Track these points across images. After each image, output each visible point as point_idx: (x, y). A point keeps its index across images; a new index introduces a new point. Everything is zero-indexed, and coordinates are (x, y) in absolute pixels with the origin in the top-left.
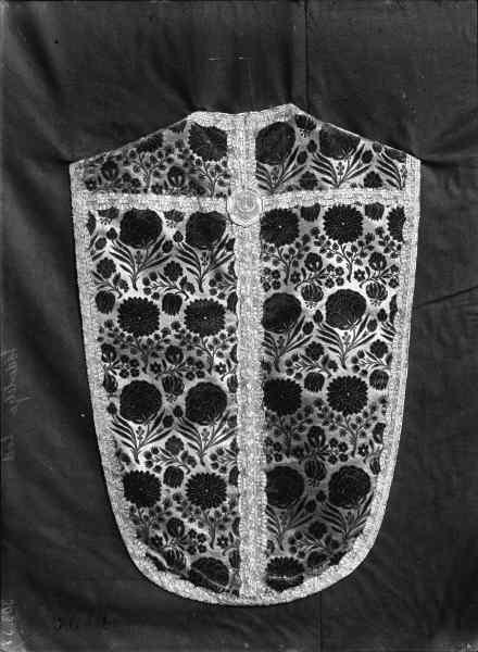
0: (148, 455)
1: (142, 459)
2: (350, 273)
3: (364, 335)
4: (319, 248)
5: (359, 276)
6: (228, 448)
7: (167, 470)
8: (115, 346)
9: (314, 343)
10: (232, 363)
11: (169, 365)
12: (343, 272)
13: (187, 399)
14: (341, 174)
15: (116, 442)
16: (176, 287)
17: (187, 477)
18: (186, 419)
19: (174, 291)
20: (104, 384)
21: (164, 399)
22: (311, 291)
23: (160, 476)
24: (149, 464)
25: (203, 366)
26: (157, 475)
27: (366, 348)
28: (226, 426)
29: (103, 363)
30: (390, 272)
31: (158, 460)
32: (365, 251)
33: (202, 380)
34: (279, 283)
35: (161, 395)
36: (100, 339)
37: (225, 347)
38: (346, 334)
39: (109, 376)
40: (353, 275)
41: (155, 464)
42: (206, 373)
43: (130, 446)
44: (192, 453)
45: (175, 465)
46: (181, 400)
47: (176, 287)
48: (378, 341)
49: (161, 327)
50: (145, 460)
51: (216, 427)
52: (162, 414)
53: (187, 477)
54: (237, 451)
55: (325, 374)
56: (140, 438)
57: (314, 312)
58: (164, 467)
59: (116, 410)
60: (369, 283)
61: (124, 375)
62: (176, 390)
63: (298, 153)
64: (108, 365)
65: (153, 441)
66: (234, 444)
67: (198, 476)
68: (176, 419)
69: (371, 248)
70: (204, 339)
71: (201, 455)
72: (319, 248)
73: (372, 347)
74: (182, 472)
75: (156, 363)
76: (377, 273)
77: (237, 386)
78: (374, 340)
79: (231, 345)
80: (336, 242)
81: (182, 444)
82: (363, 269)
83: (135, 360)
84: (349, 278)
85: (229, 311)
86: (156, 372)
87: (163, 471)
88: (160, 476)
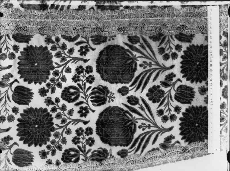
0: (165, 119)
1: (168, 124)
2: (81, 121)
3: (142, 109)
4: (57, 151)
5: (84, 112)
6: (158, 43)
7: (179, 101)
8: (64, 149)
9: (147, 95)
10: (79, 40)
11: (80, 99)
12: (81, 129)
13: (112, 83)
14: (150, 65)
15: (153, 150)
16: (7, 91)
17: (185, 82)
18: (131, 83)
19: (10, 94)
20: (100, 161)
21: (112, 104)
22: (97, 97)
23: (184, 107)
24: (173, 118)
25: (81, 67)
26: (183, 110)
27: (154, 107)
28: (137, 46)
29: (81, 161)
30: (80, 83)
31: (169, 110)
32: (60, 106)
33: (94, 69)
34: (87, 129)
35: (109, 108)
36: (58, 163)
37: (64, 47)
38: (140, 127)
39: (92, 156)
40: (83, 118)
41: (173, 112)
42: (87, 64)
43: (157, 136)
44: (162, 77)
45: (173, 93)
46: (114, 88)
47: (7, 91)
48: (147, 95)
49: (44, 106)
50: (169, 121)
51: (138, 55)
52: (126, 106)
53: (185, 82)
54: (161, 35)
55: (178, 84)
56: (149, 126)
57: (119, 157)
58: (176, 103)
59: (124, 87)
60: (90, 103)
61: (91, 142)
62: (104, 92)
63: (129, 105)
64: (82, 157)
65: (151, 114)
66: (155, 38)
67: (184, 71)
68: (130, 93)
69: (57, 100)
70: (55, 66)
71: (165, 69)
72: (57, 151)
73: (154, 102)
74: (181, 86)
75: (79, 112)
76: (82, 95)
77: (101, 36)
78: (146, 99)
79: (62, 41)
80: (52, 133)
81: (154, 87)
82: (77, 109)
83: (77, 131)
84: (85, 123)
85: (30, 42)
86: (88, 112)
87: (179, 104)
88: (184, 107)
